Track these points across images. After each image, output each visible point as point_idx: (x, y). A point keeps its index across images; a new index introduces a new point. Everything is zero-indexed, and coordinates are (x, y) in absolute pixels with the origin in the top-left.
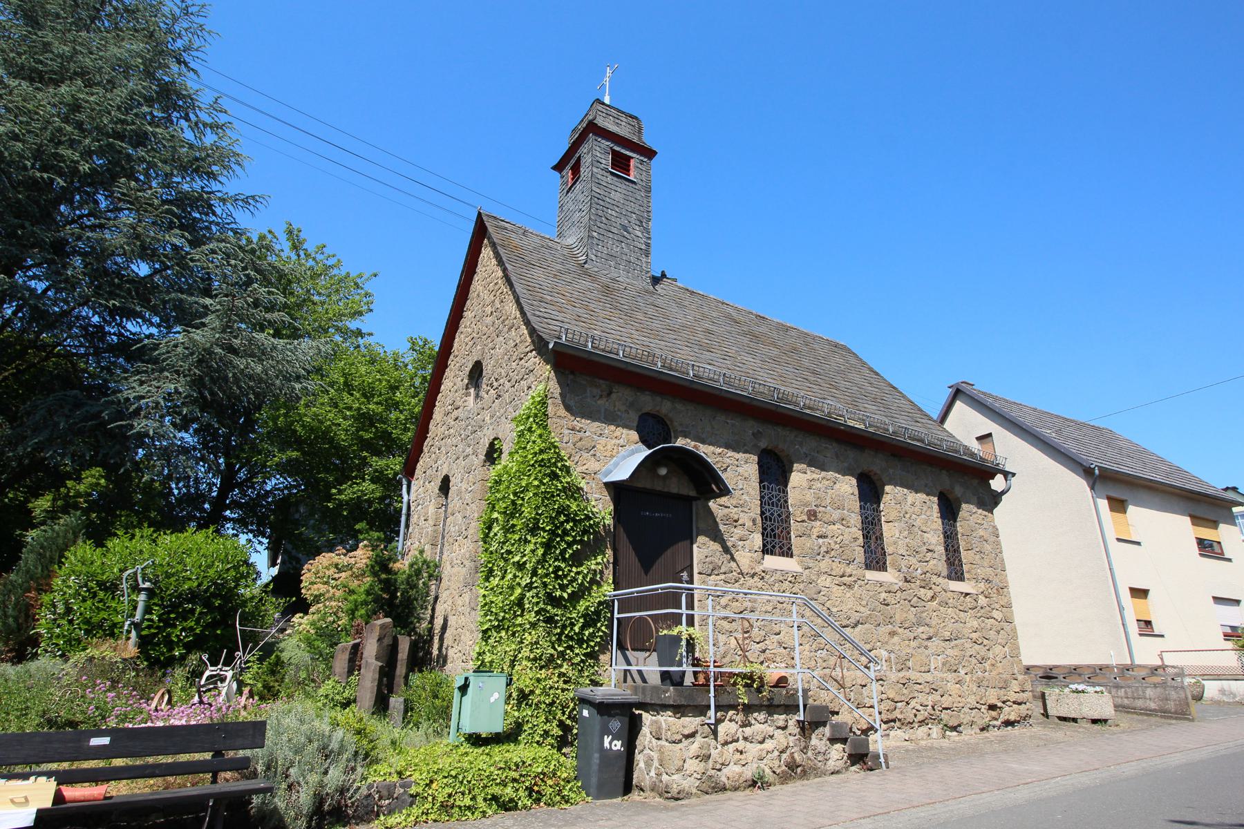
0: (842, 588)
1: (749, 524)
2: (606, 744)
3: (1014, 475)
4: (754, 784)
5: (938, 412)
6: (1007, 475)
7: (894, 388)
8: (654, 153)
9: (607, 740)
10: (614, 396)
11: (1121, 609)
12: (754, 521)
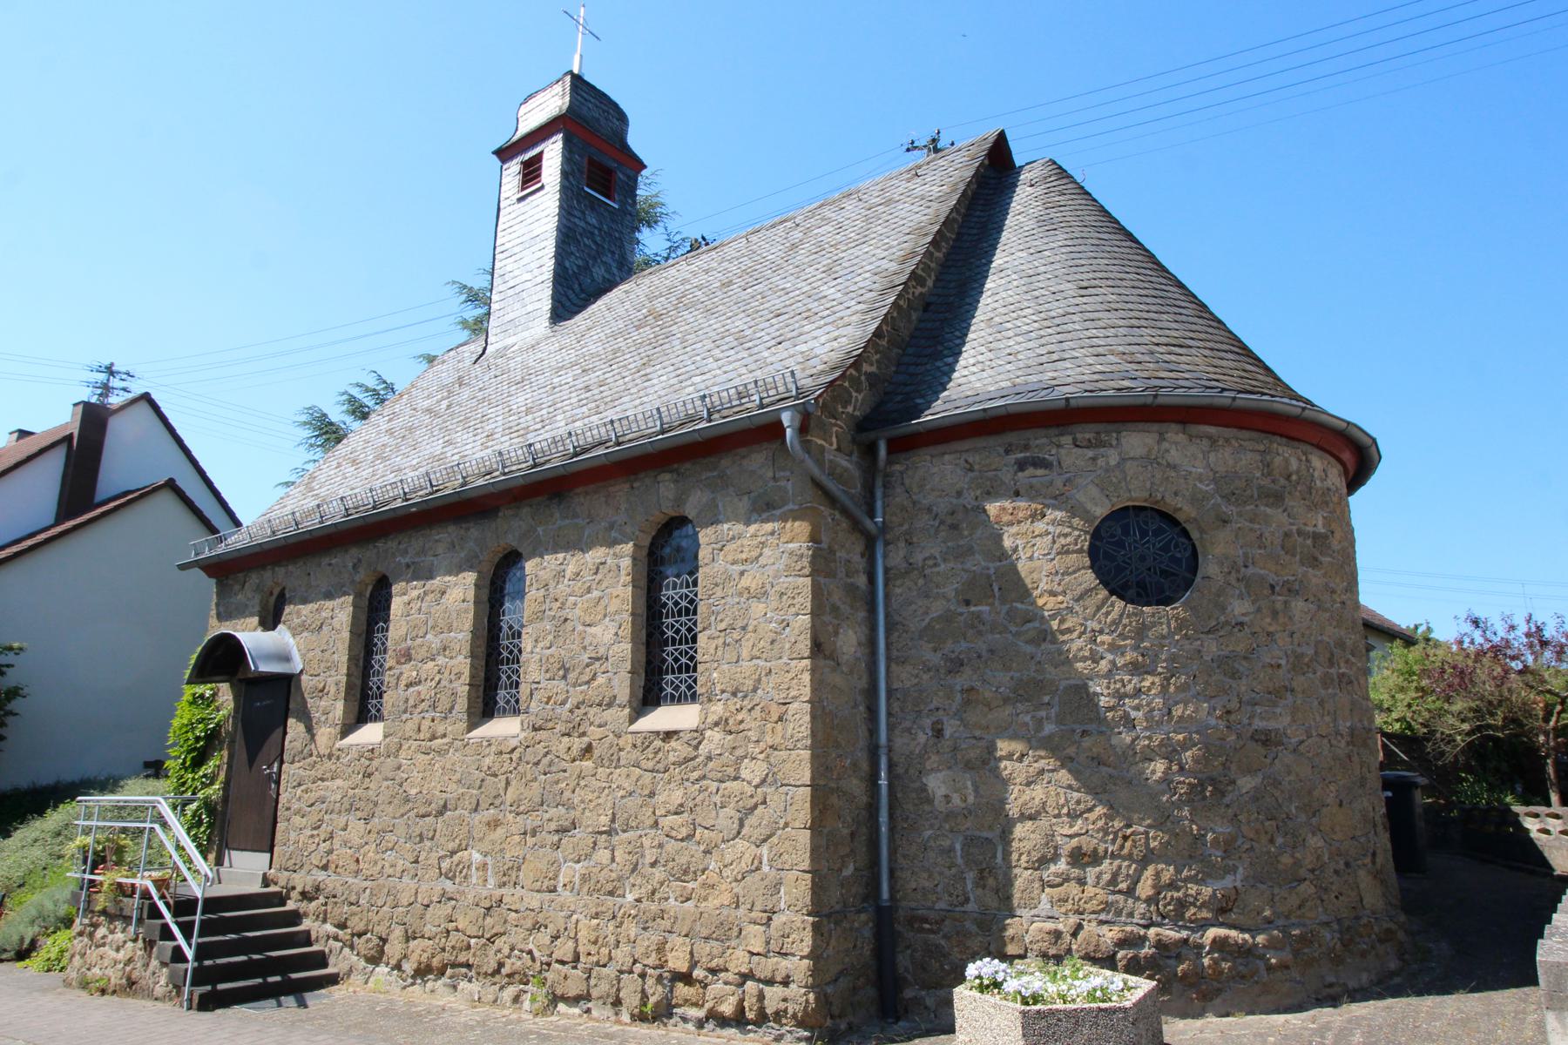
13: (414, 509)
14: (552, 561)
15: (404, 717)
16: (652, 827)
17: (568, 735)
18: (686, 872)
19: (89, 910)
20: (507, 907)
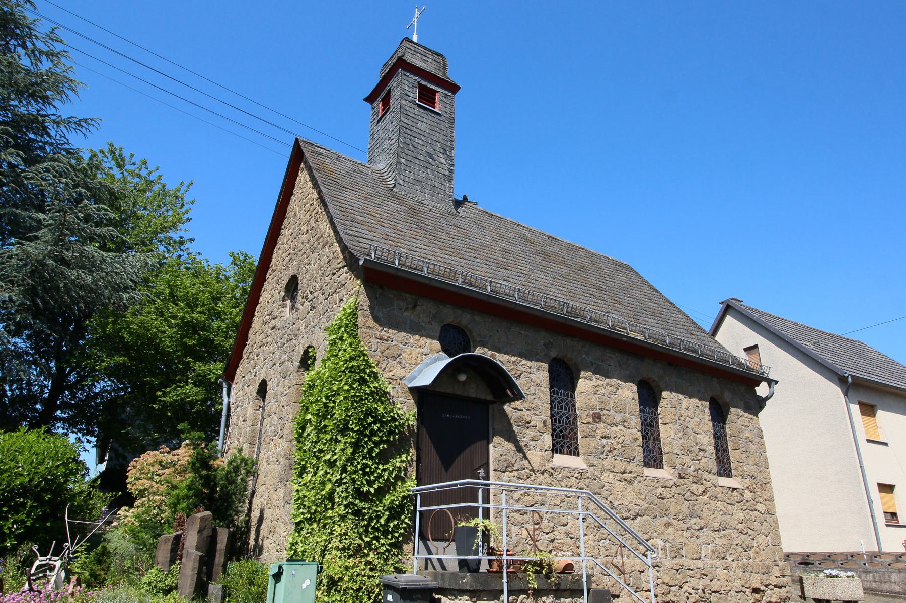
1: (540, 425)
3: (776, 382)
8: (458, 88)
10: (418, 308)
11: (870, 503)
12: (545, 423)
13: (625, 339)
14: (675, 396)
15: (603, 456)
16: (176, 198)
17: (696, 483)
18: (748, 547)
19: (41, 84)
20: (686, 568)
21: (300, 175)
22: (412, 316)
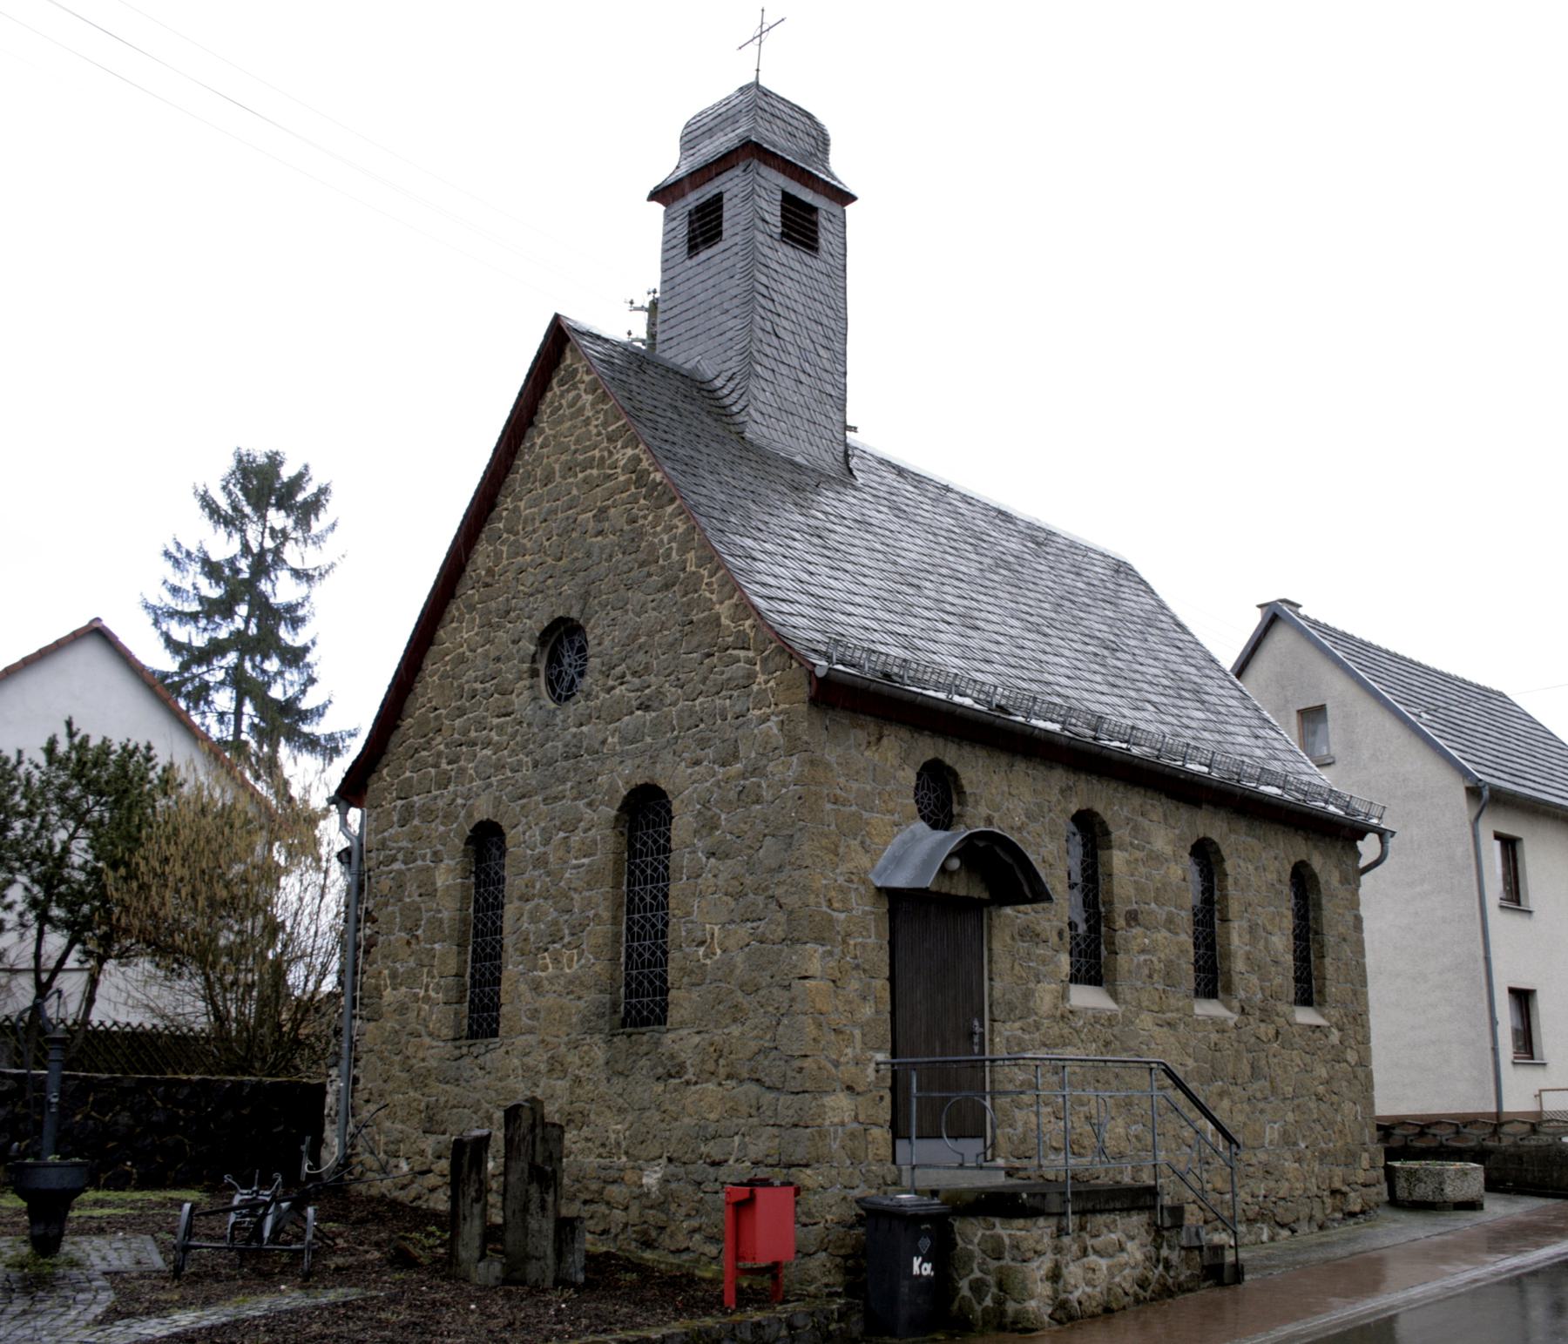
0: (1165, 1029)
1: (1054, 939)
2: (916, 1270)
3: (1393, 833)
4: (1108, 1310)
5: (1542, 1030)
6: (1382, 834)
7: (1179, 625)
8: (852, 198)
9: (916, 1262)
10: (885, 741)
11: (1494, 1023)
12: (1060, 934)
21: (556, 389)
22: (877, 757)
